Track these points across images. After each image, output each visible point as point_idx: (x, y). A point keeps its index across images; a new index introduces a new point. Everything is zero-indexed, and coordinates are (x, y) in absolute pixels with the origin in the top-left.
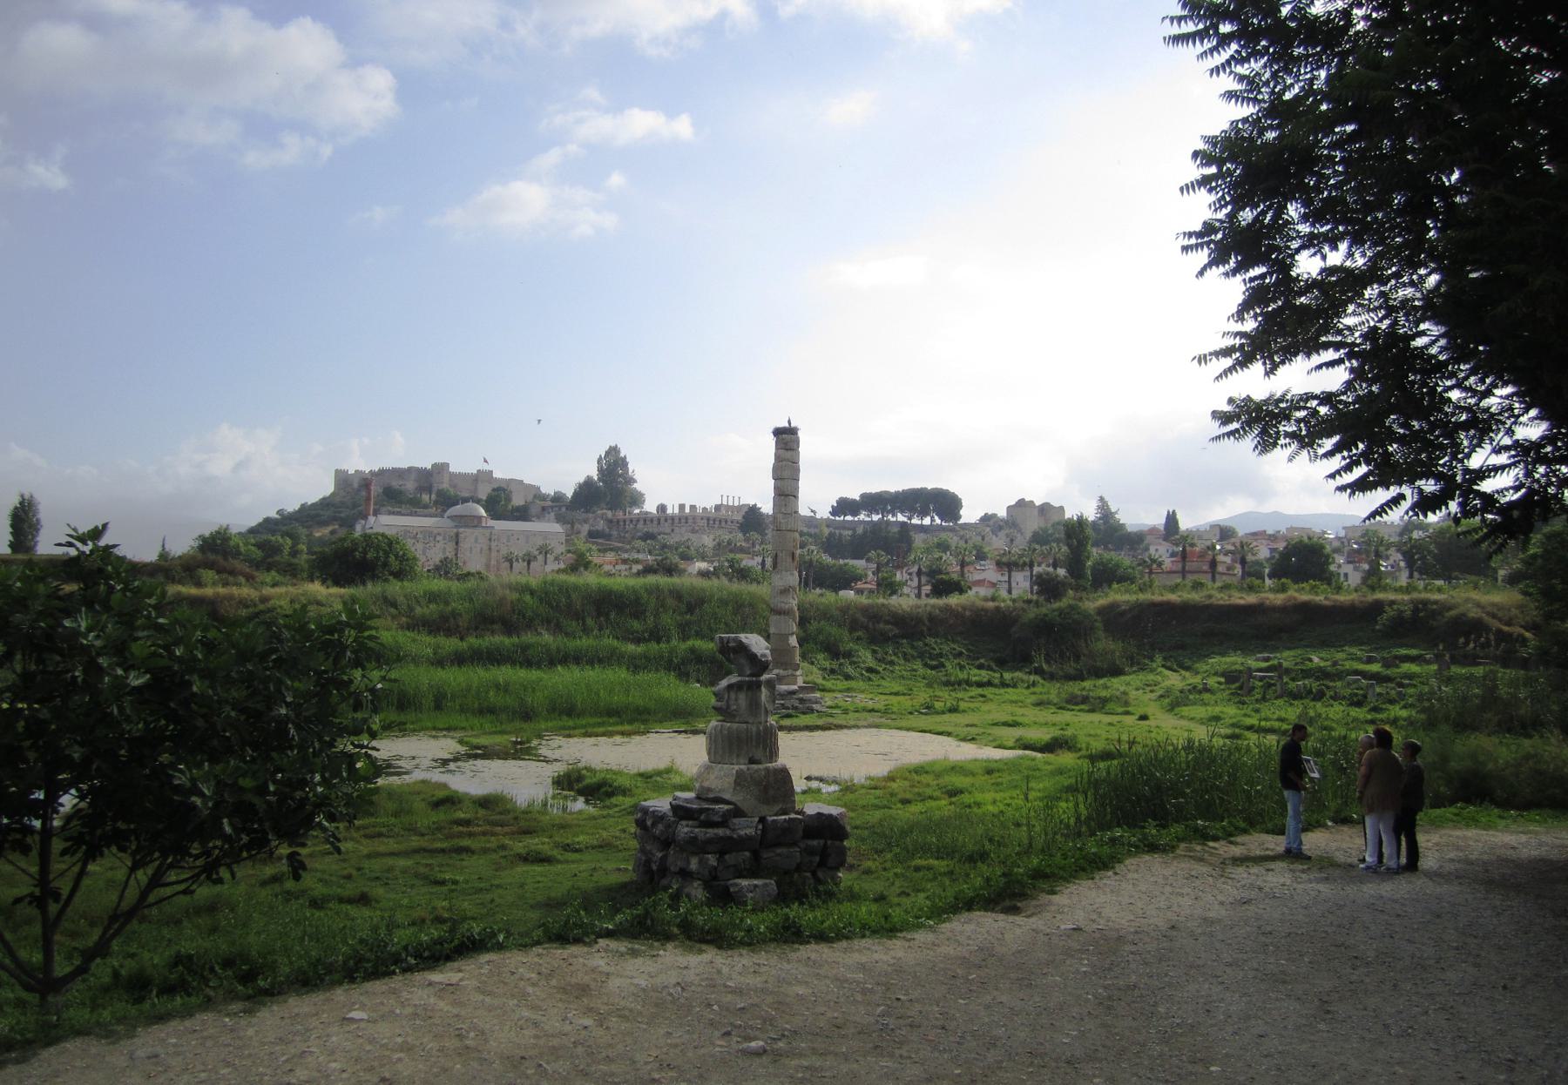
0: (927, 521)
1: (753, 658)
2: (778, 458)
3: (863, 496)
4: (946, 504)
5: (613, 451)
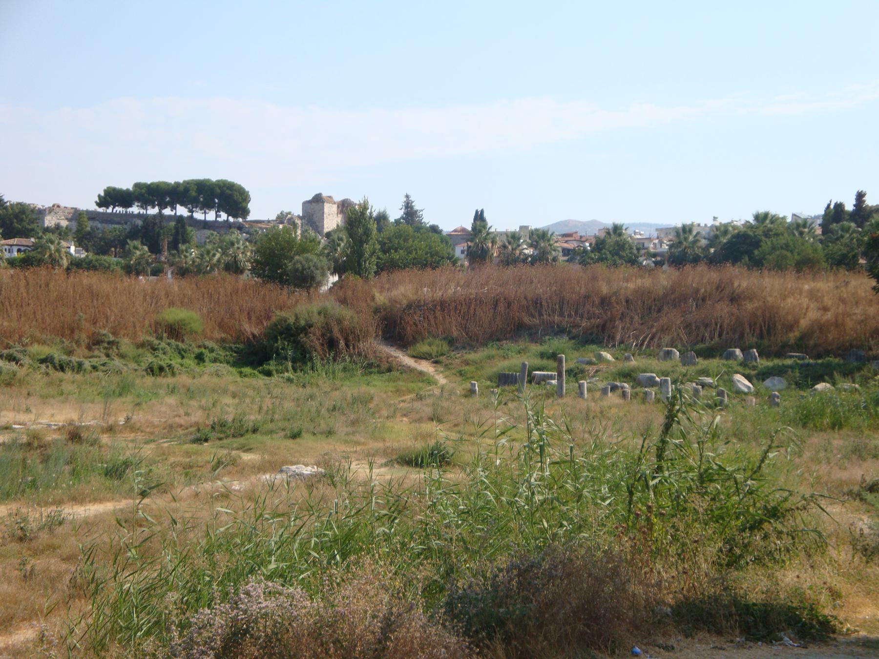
0: (211, 216)
3: (137, 186)
4: (229, 197)
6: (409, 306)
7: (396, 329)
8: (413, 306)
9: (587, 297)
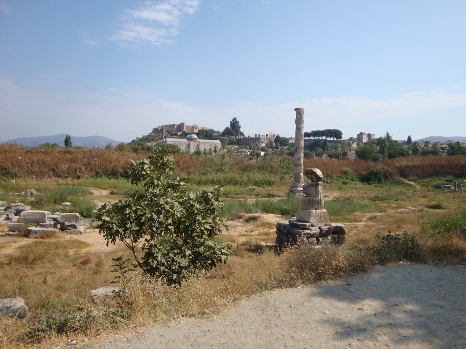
0: (332, 139)
1: (317, 176)
2: (297, 117)
3: (312, 131)
4: (337, 134)
5: (235, 119)
6: (406, 167)
7: (404, 173)
8: (407, 167)
9: (458, 165)
